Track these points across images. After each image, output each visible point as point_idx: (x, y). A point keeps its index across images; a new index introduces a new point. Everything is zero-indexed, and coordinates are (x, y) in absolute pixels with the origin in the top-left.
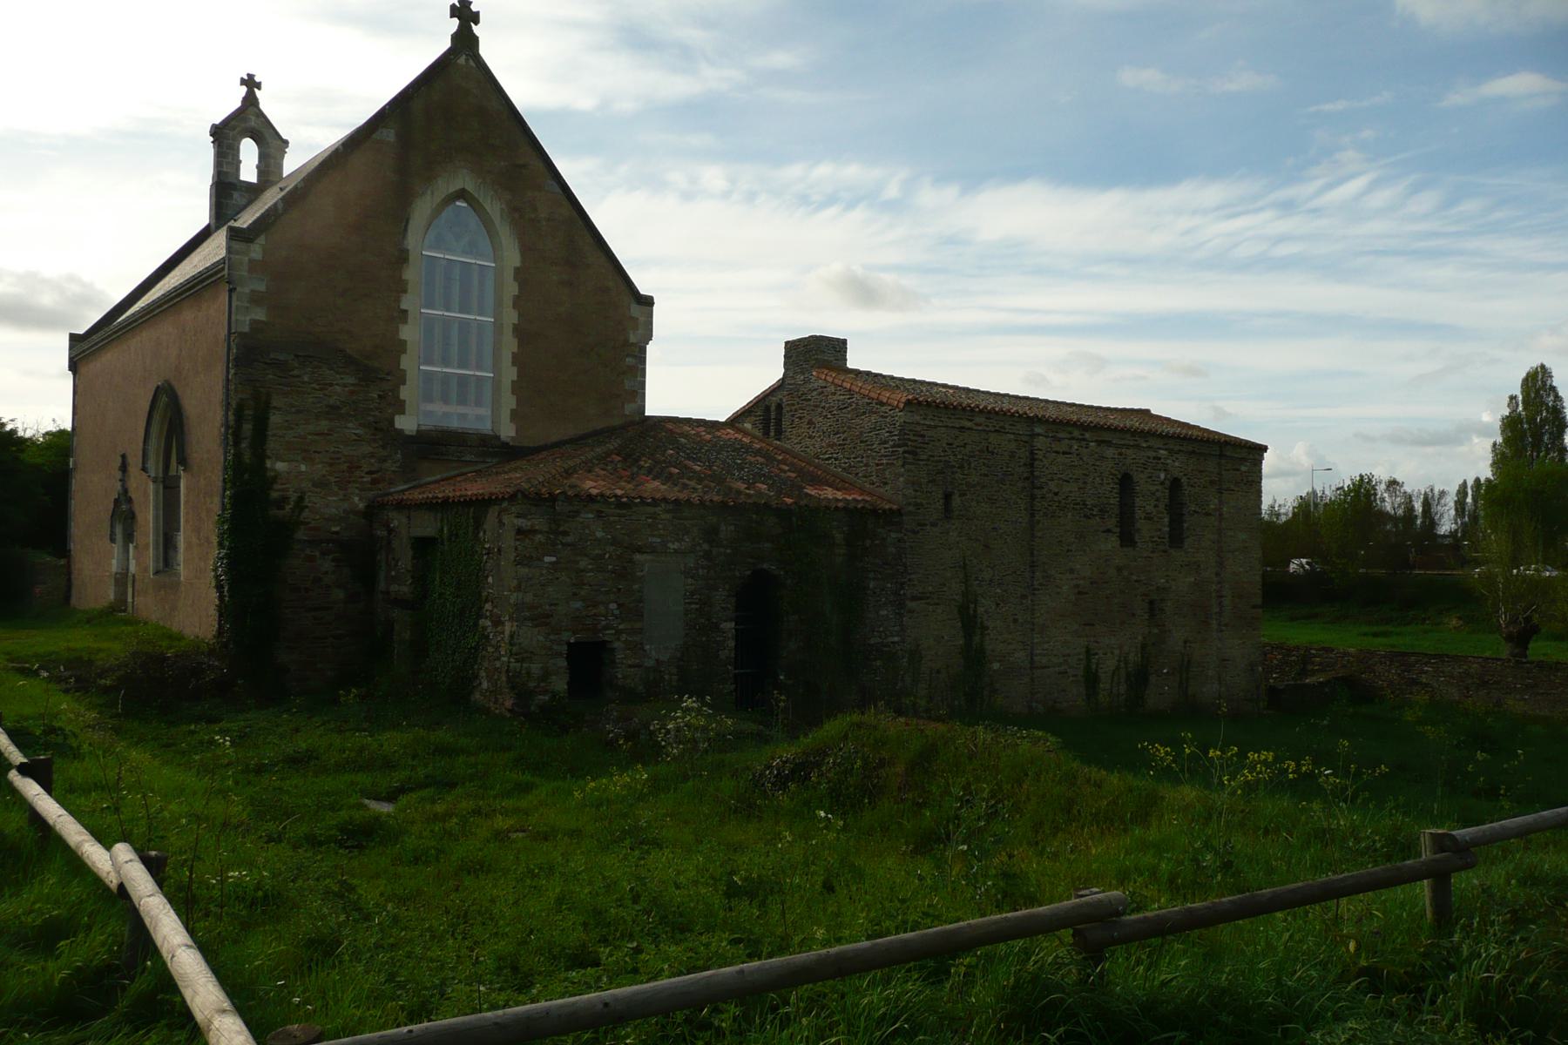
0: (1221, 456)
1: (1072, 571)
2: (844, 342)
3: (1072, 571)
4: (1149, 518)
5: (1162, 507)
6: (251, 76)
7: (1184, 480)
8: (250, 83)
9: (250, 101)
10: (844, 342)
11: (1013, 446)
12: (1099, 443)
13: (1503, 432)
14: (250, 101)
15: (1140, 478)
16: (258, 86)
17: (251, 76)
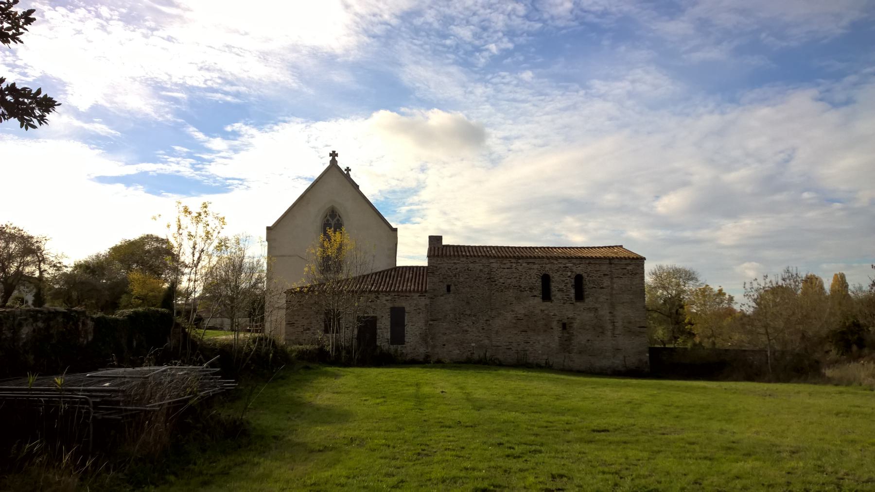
0: (611, 264)
1: (513, 311)
2: (430, 237)
3: (513, 311)
4: (560, 290)
5: (569, 285)
6: (334, 152)
7: (585, 275)
8: (334, 155)
9: (334, 163)
10: (430, 237)
11: (481, 268)
12: (528, 263)
13: (78, 266)
14: (334, 163)
15: (555, 277)
16: (337, 155)
17: (334, 152)
